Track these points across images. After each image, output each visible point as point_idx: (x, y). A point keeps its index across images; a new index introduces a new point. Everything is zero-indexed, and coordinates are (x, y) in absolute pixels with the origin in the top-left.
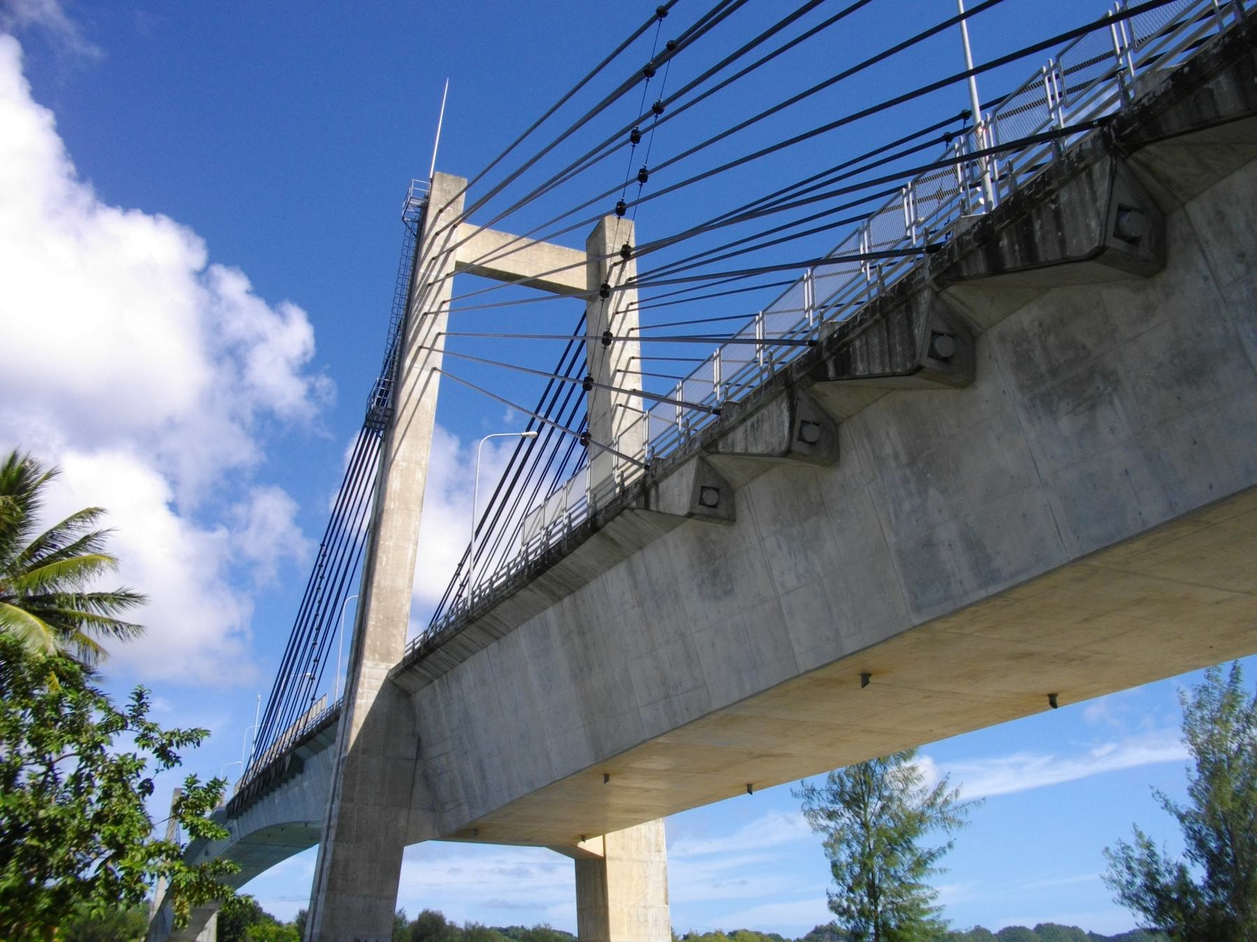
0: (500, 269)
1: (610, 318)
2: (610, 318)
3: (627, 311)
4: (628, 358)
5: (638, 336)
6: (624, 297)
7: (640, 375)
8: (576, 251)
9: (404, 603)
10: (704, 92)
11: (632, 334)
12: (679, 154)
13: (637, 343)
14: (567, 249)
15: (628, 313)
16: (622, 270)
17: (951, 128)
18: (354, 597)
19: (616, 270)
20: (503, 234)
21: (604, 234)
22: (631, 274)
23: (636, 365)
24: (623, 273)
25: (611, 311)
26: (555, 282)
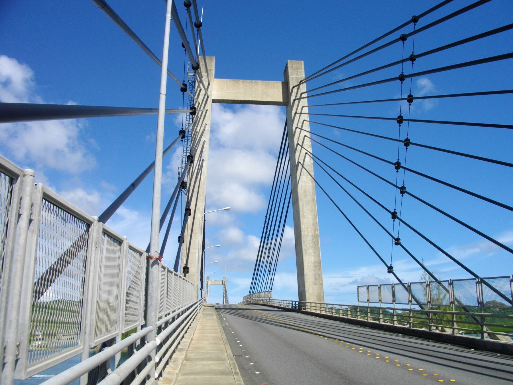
0: (236, 99)
1: (294, 130)
2: (294, 130)
3: (301, 98)
4: (303, 136)
5: (306, 96)
6: (300, 103)
7: (308, 115)
8: (275, 82)
9: (196, 280)
10: (406, 354)
11: (303, 96)
12: (343, 215)
13: (306, 100)
14: (270, 82)
15: (302, 100)
16: (298, 89)
17: (406, 30)
18: (200, 172)
19: (295, 89)
20: (237, 80)
21: (288, 71)
22: (303, 90)
23: (306, 110)
24: (299, 90)
25: (294, 128)
26: (265, 100)
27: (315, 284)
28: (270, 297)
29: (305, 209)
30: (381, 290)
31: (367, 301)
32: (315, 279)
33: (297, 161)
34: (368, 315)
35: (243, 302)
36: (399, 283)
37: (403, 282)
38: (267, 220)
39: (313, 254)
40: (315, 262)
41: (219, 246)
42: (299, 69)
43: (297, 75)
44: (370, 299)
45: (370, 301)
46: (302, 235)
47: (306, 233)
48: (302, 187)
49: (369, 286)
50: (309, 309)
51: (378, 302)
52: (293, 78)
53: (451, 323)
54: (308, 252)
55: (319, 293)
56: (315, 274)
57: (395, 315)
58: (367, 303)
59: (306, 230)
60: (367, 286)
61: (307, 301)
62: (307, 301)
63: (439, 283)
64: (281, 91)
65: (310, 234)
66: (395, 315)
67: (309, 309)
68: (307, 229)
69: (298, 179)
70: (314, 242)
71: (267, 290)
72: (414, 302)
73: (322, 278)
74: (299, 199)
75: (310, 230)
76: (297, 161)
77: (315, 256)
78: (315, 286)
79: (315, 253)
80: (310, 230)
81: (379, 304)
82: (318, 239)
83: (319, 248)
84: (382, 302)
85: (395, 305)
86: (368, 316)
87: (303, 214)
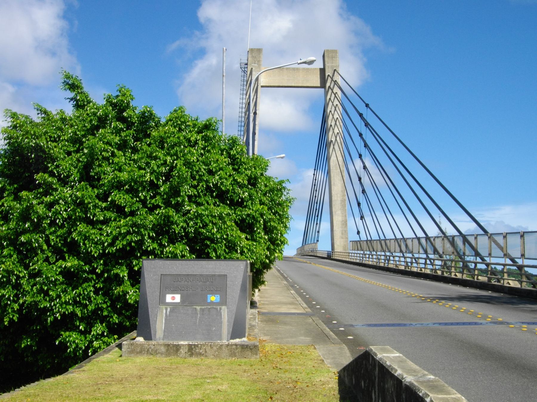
27: (342, 238)
28: (376, 250)
29: (335, 178)
30: (524, 239)
31: (488, 255)
32: (342, 234)
33: (330, 140)
34: (503, 276)
35: (296, 255)
36: (458, 234)
37: (490, 231)
38: (315, 173)
39: (341, 215)
40: (343, 221)
41: (282, 158)
42: (334, 57)
43: (333, 63)
44: (526, 253)
45: (493, 255)
46: (333, 200)
47: (336, 198)
48: (333, 161)
49: (477, 235)
50: (416, 267)
51: (520, 257)
52: (328, 67)
53: (520, 276)
54: (337, 213)
55: (345, 245)
56: (342, 231)
57: (505, 272)
58: (504, 259)
59: (336, 196)
60: (475, 236)
61: (335, 251)
62: (335, 251)
63: (491, 237)
64: (319, 76)
65: (339, 199)
66: (505, 272)
67: (416, 267)
68: (337, 194)
69: (331, 154)
70: (342, 205)
71: (315, 242)
72: (456, 253)
73: (347, 233)
74: (331, 171)
75: (339, 195)
76: (330, 140)
77: (342, 216)
78: (342, 240)
79: (343, 214)
80: (339, 195)
81: (504, 259)
82: (345, 202)
83: (346, 210)
84: (526, 257)
85: (525, 260)
86: (504, 278)
87: (334, 183)
